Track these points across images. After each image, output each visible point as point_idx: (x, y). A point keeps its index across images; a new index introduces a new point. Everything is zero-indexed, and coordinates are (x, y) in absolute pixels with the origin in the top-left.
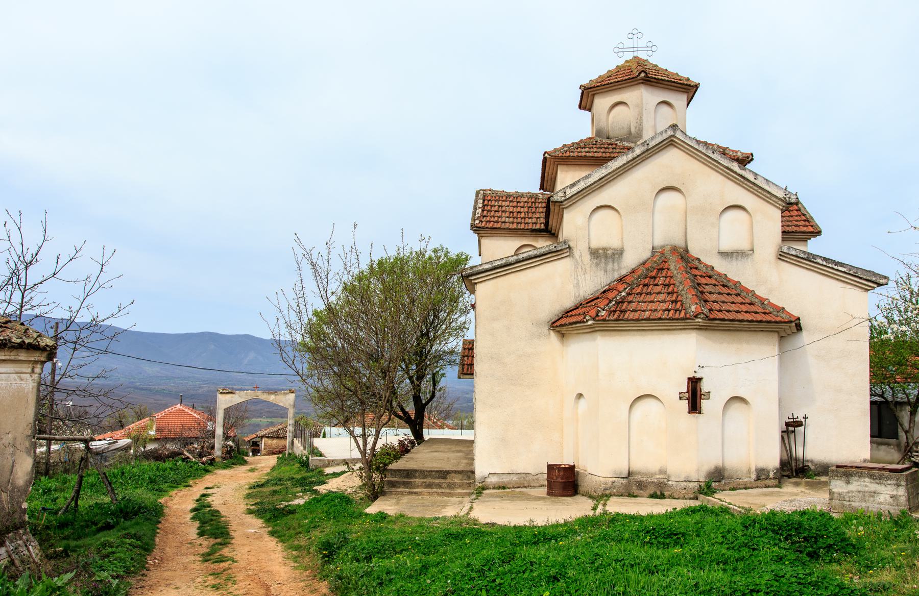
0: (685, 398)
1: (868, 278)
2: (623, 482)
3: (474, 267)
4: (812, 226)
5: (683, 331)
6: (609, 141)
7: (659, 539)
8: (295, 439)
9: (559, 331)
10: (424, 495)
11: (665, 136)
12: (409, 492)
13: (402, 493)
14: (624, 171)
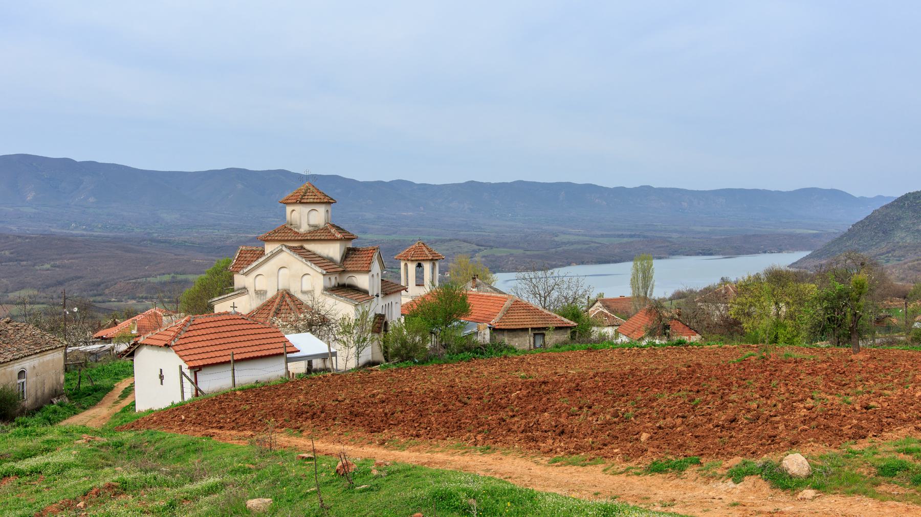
4: (297, 301)
11: (279, 249)
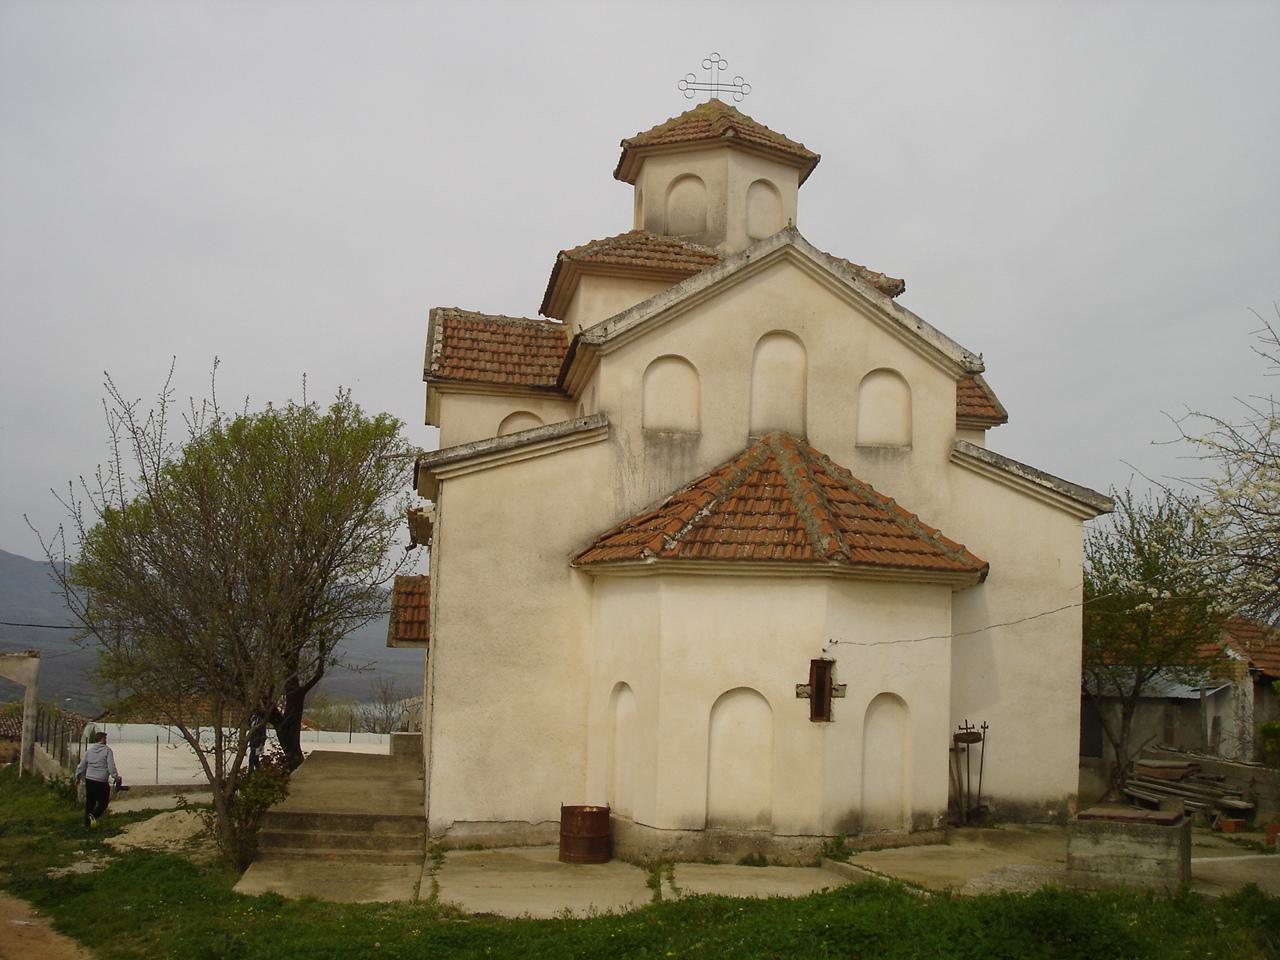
0: (806, 695)
1: (1084, 500)
2: (697, 838)
4: (993, 407)
6: (669, 241)
7: (842, 945)
8: (38, 744)
10: (332, 860)
11: (776, 245)
12: (306, 855)
13: (292, 857)
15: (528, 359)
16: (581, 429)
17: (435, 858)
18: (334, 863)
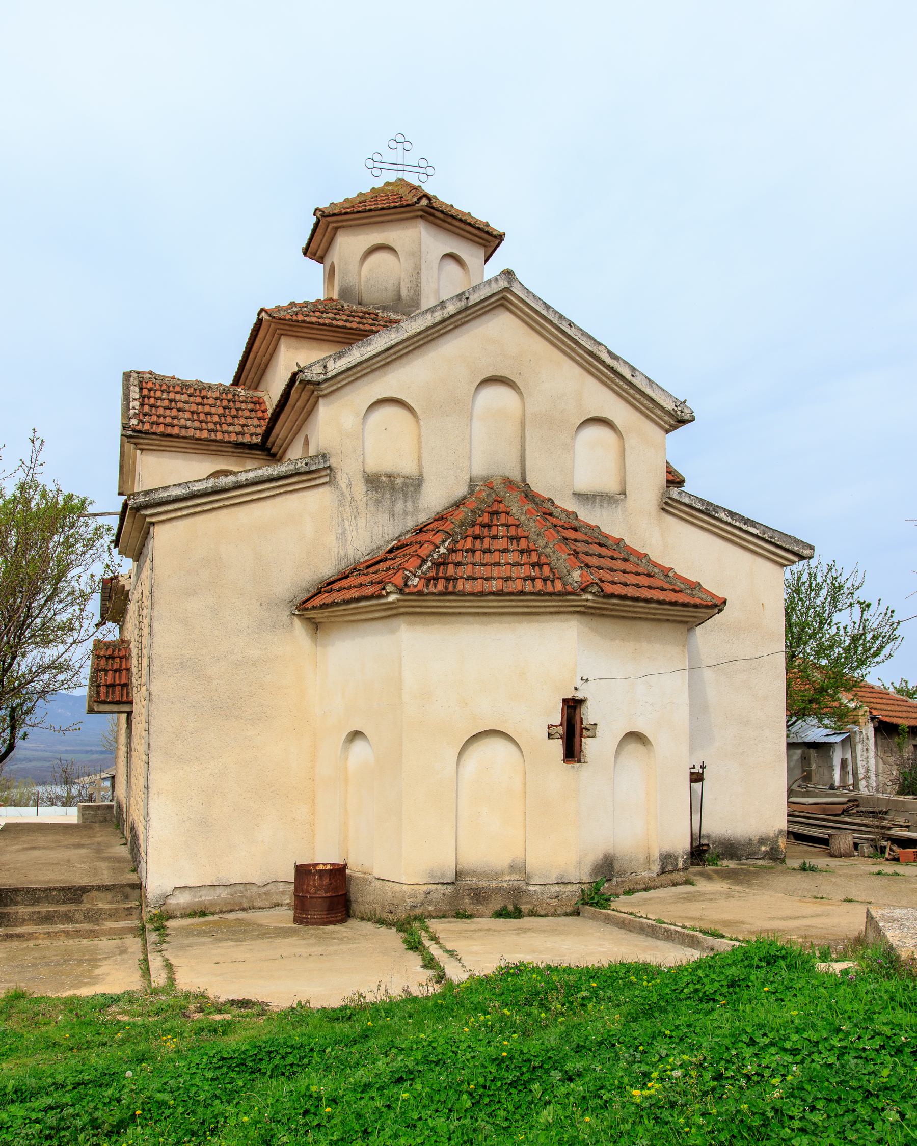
0: (558, 736)
1: (787, 547)
2: (447, 892)
3: (151, 491)
5: (555, 617)
9: (309, 619)
10: (37, 938)
11: (495, 288)
12: (7, 935)
14: (426, 340)
15: (229, 420)
16: (303, 470)
17: (157, 929)
18: (40, 942)
